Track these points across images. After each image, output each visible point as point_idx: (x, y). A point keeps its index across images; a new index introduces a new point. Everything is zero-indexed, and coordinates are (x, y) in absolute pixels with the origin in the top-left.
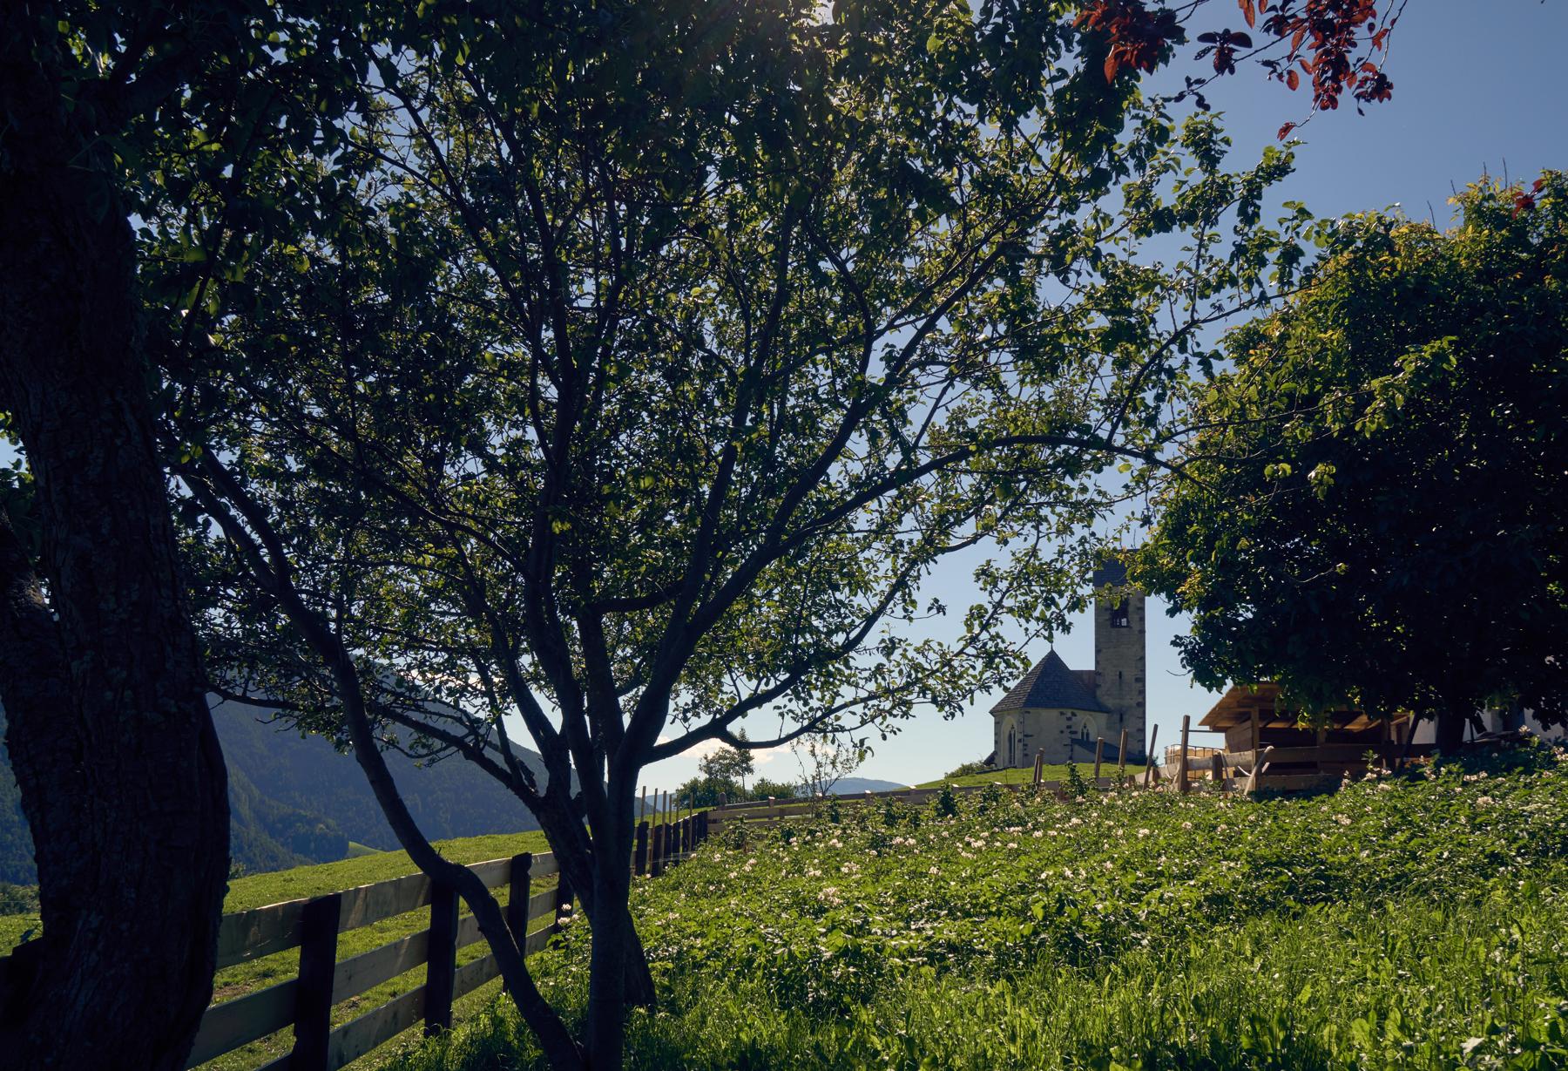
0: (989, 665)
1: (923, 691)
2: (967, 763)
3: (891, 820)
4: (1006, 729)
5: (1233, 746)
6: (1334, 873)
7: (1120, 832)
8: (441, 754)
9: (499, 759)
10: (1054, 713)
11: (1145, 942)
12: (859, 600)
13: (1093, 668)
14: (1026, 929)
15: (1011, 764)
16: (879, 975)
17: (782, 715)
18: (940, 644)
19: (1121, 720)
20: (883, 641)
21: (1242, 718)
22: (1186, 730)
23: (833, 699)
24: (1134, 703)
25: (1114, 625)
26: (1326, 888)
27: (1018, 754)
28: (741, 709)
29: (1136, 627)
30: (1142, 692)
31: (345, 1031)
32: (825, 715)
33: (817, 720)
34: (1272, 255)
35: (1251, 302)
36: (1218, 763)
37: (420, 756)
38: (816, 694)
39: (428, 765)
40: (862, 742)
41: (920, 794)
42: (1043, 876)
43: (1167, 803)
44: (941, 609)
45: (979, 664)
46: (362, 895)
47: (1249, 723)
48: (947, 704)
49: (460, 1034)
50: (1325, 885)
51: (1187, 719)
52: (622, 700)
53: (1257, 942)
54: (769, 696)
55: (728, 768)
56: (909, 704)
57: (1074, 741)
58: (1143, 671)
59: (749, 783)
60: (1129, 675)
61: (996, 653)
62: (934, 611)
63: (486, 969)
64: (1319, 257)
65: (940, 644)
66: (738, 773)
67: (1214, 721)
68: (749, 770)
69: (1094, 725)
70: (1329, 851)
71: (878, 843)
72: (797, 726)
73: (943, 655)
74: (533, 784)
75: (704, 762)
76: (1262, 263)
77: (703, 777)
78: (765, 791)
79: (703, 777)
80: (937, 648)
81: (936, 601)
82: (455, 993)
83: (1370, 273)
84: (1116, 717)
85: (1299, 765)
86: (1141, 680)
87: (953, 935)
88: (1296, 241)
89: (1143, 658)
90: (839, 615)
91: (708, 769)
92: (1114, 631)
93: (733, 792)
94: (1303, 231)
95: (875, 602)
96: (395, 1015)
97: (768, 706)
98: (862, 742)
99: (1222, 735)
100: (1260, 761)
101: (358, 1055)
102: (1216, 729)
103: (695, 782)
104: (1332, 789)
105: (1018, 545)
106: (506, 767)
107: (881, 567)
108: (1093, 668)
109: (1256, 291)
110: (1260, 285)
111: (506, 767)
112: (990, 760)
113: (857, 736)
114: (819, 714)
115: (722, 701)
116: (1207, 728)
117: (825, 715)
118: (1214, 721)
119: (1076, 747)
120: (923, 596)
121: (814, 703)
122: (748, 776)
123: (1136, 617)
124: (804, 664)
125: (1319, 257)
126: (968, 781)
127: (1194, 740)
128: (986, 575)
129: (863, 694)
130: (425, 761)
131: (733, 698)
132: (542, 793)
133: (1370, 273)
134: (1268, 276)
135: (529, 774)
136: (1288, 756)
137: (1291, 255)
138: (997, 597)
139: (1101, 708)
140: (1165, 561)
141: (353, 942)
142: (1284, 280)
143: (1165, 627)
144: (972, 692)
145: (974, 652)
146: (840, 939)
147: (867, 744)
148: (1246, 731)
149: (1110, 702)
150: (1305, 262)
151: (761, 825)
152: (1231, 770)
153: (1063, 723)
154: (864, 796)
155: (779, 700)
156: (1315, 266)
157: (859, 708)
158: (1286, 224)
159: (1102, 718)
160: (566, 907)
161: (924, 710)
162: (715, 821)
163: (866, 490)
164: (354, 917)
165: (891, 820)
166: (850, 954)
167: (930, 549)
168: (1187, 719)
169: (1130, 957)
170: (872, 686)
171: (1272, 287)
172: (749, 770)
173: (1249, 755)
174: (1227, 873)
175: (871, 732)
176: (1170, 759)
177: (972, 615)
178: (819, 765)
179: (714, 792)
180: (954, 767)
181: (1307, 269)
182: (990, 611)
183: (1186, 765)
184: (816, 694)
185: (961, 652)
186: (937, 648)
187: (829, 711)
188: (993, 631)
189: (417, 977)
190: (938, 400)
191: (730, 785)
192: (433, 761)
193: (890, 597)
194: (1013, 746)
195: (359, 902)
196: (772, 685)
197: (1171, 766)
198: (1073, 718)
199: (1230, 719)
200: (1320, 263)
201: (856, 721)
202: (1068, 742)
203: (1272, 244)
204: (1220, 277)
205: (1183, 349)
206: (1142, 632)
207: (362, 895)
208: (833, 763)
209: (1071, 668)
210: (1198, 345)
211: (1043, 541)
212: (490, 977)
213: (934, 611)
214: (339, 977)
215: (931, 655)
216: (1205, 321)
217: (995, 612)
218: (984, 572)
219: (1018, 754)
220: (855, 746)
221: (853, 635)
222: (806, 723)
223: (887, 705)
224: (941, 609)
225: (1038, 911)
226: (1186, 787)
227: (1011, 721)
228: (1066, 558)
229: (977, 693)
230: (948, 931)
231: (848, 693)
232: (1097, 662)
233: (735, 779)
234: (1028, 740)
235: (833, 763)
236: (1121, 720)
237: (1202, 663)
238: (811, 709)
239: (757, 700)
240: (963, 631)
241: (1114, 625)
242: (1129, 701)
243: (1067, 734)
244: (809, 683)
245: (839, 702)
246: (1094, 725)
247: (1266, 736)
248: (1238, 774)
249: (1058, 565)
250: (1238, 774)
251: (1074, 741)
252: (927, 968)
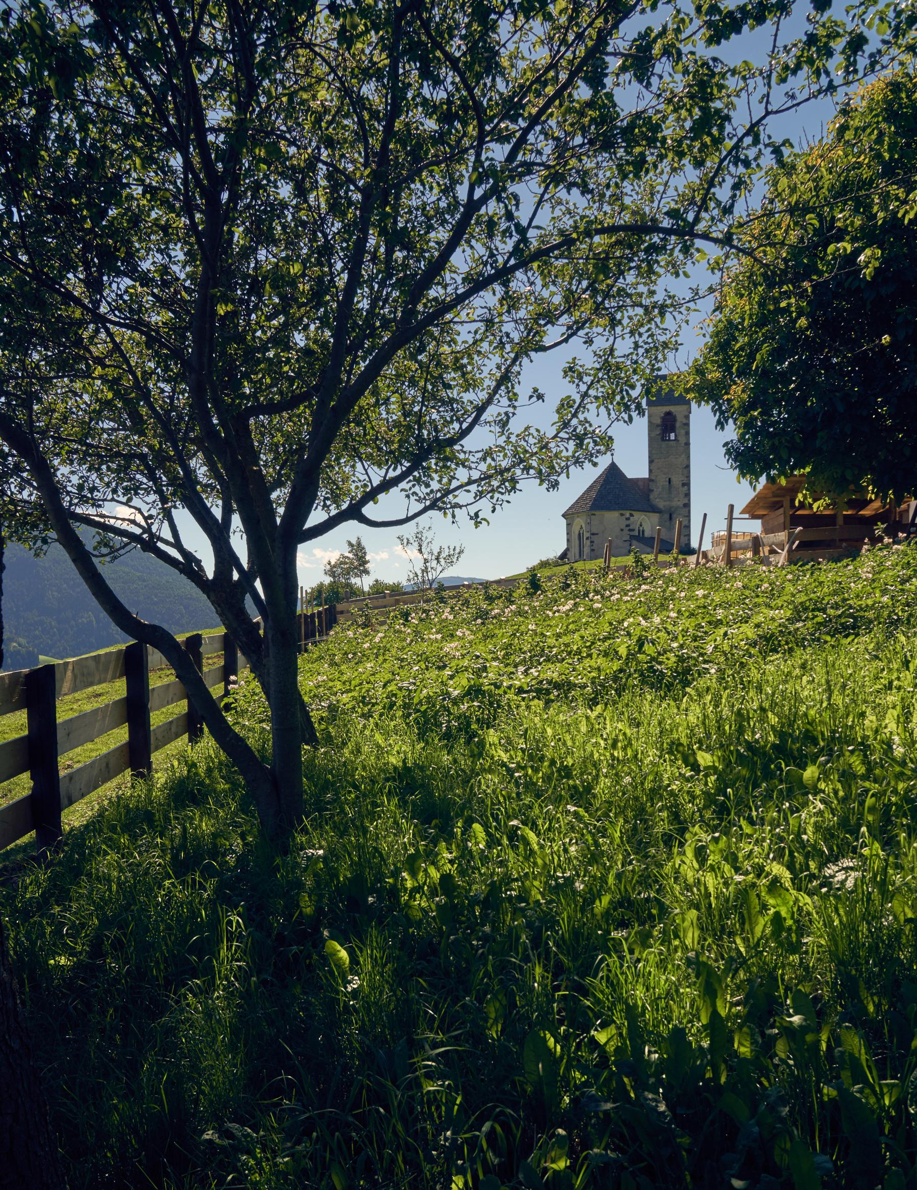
0: (580, 445)
1: (527, 469)
2: (544, 559)
3: (490, 599)
4: (576, 529)
5: (767, 530)
6: (862, 613)
7: (683, 594)
8: (122, 552)
9: (174, 553)
10: (615, 514)
11: (713, 671)
12: (467, 397)
13: (646, 475)
14: (616, 665)
15: (581, 557)
16: (499, 706)
17: (408, 496)
18: (538, 431)
19: (671, 518)
20: (499, 414)
21: (775, 506)
22: (731, 518)
23: (450, 481)
24: (680, 504)
25: (663, 439)
26: (854, 627)
27: (586, 550)
28: (371, 495)
29: (682, 440)
30: (688, 495)
31: (71, 777)
32: (443, 496)
33: (437, 500)
34: (839, 45)
35: (820, 92)
36: (756, 543)
37: (103, 556)
38: (436, 476)
39: (112, 561)
40: (477, 515)
41: (510, 583)
42: (626, 624)
43: (717, 576)
44: (540, 397)
45: (571, 445)
46: (70, 667)
47: (781, 510)
48: (549, 478)
49: (160, 778)
50: (851, 625)
51: (732, 507)
52: (274, 496)
53: (803, 666)
54: (395, 481)
55: (348, 572)
56: (514, 481)
57: (632, 537)
58: (688, 477)
59: (365, 583)
60: (677, 480)
61: (585, 434)
62: (535, 399)
63: (174, 729)
64: (884, 42)
65: (538, 431)
66: (356, 575)
67: (752, 511)
68: (367, 572)
69: (649, 523)
70: (858, 596)
71: (483, 615)
72: (422, 506)
73: (541, 440)
74: (201, 569)
75: (328, 567)
76: (830, 53)
77: (327, 580)
78: (379, 589)
79: (327, 580)
80: (535, 434)
81: (535, 390)
82: (152, 747)
83: (903, 95)
84: (667, 516)
85: (825, 540)
86: (687, 484)
87: (555, 675)
88: (863, 29)
89: (688, 467)
90: (452, 410)
91: (331, 572)
92: (664, 444)
93: (353, 592)
94: (868, 18)
95: (483, 395)
96: (107, 765)
97: (394, 491)
98: (477, 515)
99: (760, 521)
100: (791, 539)
101: (83, 796)
102: (754, 517)
103: (321, 585)
104: (854, 554)
105: (601, 343)
106: (181, 559)
107: (489, 366)
108: (646, 475)
109: (824, 81)
110: (827, 73)
111: (181, 559)
112: (564, 556)
113: (472, 510)
114: (439, 495)
115: (355, 489)
116: (747, 516)
117: (443, 496)
118: (752, 511)
119: (634, 542)
120: (523, 390)
121: (435, 485)
122: (364, 577)
123: (683, 432)
124: (423, 452)
125: (884, 42)
126: (547, 572)
127: (737, 526)
128: (572, 371)
129: (476, 475)
130: (108, 559)
131: (365, 486)
132: (210, 575)
133: (903, 95)
134: (836, 65)
135: (198, 562)
136: (813, 536)
137: (857, 43)
138: (583, 388)
139: (654, 510)
140: (714, 375)
141: (66, 709)
142: (850, 68)
143: (709, 437)
144: (568, 467)
145: (567, 436)
146: (463, 681)
147: (481, 515)
148: (779, 516)
149: (661, 504)
150: (869, 49)
151: (382, 613)
152: (767, 549)
153: (624, 523)
154: (464, 585)
155: (404, 485)
156: (879, 51)
157: (473, 488)
158: (852, 13)
159: (655, 517)
160: (233, 678)
161: (529, 485)
162: (342, 612)
163: (477, 284)
164: (66, 685)
165: (490, 599)
166: (474, 692)
167: (531, 345)
168: (732, 507)
169: (701, 683)
170: (483, 467)
171: (838, 76)
172: (367, 572)
173: (782, 536)
174: (775, 616)
175: (484, 505)
176: (716, 542)
177: (563, 405)
178: (426, 561)
179: (337, 593)
180: (535, 562)
181: (872, 55)
182: (578, 401)
183: (730, 547)
184: (436, 476)
185: (556, 436)
186: (535, 434)
187: (448, 492)
188: (581, 417)
189: (121, 735)
190: (543, 195)
191: (348, 585)
192: (115, 558)
193: (497, 388)
194: (583, 543)
195: (69, 674)
196: (398, 471)
197: (717, 549)
198: (631, 517)
199: (764, 508)
200: (884, 48)
201: (470, 498)
202: (628, 538)
203: (838, 35)
204: (798, 58)
205: (756, 141)
206: (688, 444)
207: (70, 667)
208: (437, 559)
209: (629, 476)
210: (769, 137)
211: (619, 340)
212: (177, 736)
213: (535, 399)
214: (60, 734)
215: (531, 440)
216: (777, 112)
217: (582, 401)
218: (571, 369)
219: (586, 550)
220: (471, 518)
221: (465, 425)
222: (428, 503)
223: (495, 483)
224: (540, 397)
225: (623, 651)
226: (730, 563)
227: (580, 522)
228: (641, 351)
229: (572, 468)
230: (552, 672)
231: (462, 475)
232: (650, 471)
233: (355, 581)
234: (594, 538)
235: (437, 559)
236: (671, 518)
237: (746, 460)
238: (432, 491)
239: (386, 485)
240: (556, 417)
241: (663, 439)
242: (678, 502)
243: (626, 532)
244: (429, 468)
245: (455, 484)
246: (649, 523)
247: (795, 520)
248: (772, 552)
249: (635, 357)
250: (772, 552)
251: (632, 537)
252: (536, 701)
